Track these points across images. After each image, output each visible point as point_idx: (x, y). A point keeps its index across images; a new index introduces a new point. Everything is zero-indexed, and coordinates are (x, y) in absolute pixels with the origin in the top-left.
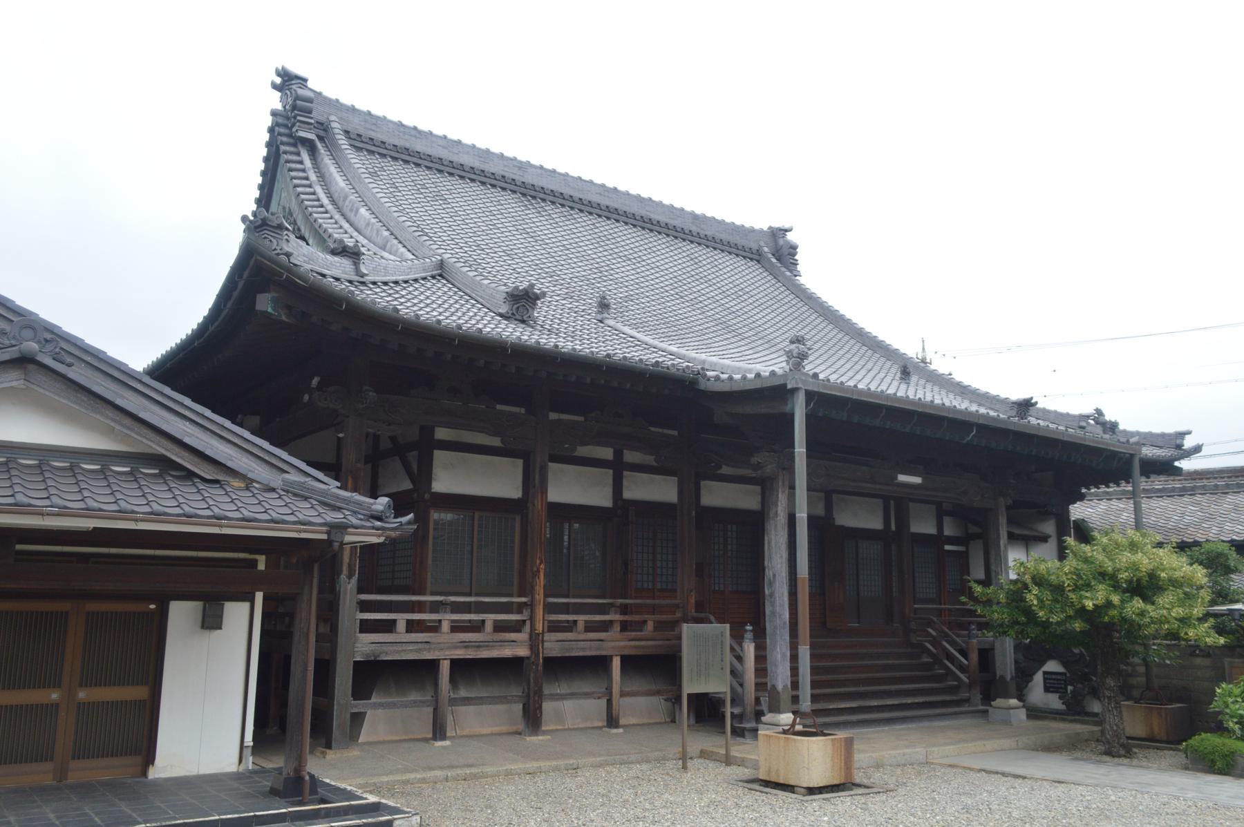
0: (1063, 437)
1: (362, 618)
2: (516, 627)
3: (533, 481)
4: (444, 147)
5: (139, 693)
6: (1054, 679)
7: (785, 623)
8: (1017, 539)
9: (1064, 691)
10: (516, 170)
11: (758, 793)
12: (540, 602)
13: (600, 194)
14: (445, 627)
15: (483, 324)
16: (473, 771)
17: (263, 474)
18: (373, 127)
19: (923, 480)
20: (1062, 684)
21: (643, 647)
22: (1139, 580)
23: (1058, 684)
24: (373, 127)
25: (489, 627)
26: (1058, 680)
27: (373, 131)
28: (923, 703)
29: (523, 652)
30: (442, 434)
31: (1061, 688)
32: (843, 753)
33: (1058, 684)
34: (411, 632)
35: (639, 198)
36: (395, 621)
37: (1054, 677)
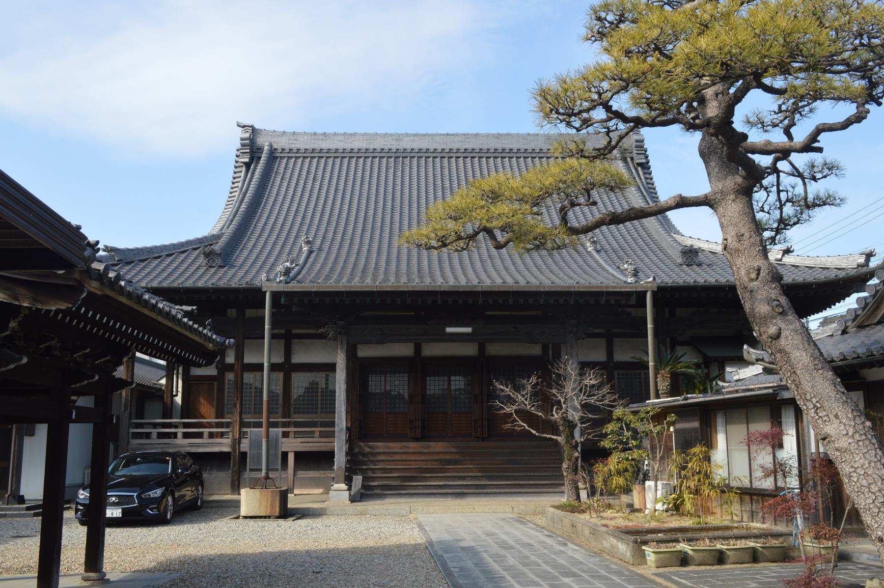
2: (222, 435)
3: (418, 348)
4: (342, 141)
7: (342, 429)
8: (734, 360)
10: (394, 142)
12: (236, 420)
13: (462, 142)
14: (180, 435)
16: (615, 541)
18: (295, 142)
19: (444, 330)
21: (316, 447)
24: (295, 142)
25: (206, 435)
27: (294, 144)
28: (170, 428)
29: (226, 449)
30: (295, 331)
32: (269, 499)
35: (498, 136)
36: (151, 433)
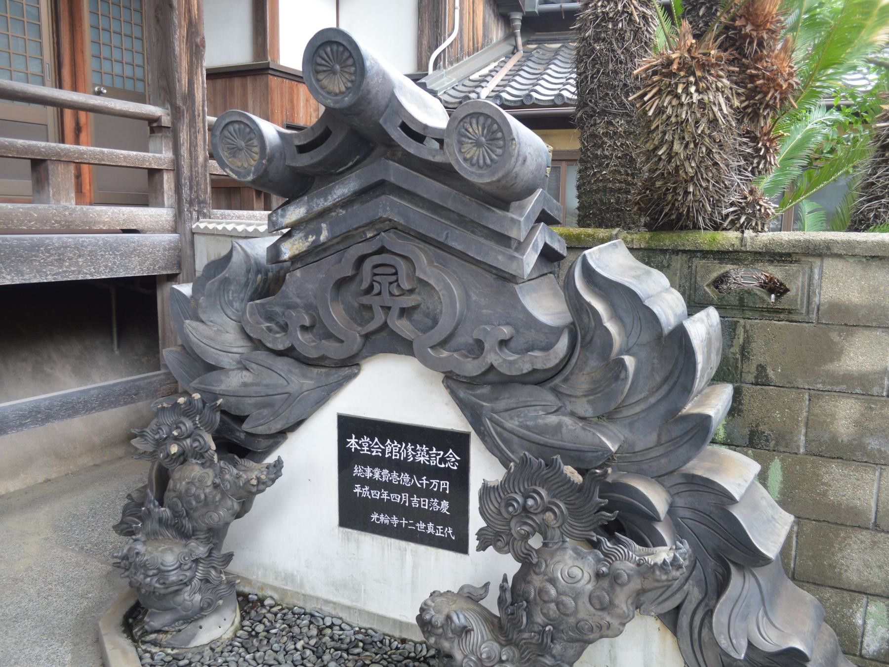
0: (150, 164)
1: (161, 209)
5: (88, 200)
6: (399, 466)
9: (357, 471)
11: (92, 162)
15: (233, 505)
17: (746, 285)
20: (441, 496)
22: (579, 216)
23: (413, 491)
26: (416, 469)
31: (437, 518)
33: (413, 491)
34: (541, 213)
37: (393, 449)
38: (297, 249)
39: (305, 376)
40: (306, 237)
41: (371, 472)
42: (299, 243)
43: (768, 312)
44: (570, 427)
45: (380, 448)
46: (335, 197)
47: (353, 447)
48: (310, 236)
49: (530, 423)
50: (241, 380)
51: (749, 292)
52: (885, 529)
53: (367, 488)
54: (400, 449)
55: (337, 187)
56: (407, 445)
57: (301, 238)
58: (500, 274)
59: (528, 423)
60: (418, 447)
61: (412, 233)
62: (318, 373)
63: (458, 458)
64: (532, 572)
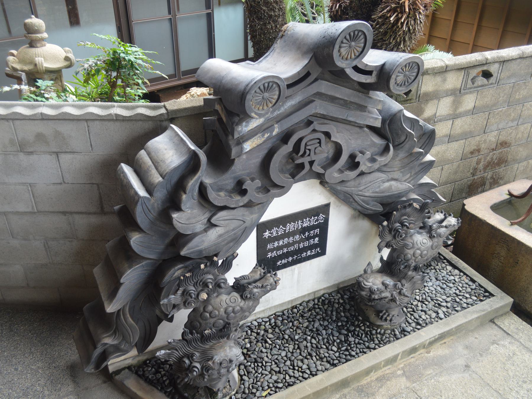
38: (256, 144)
39: (252, 213)
40: (263, 135)
41: (278, 243)
42: (257, 140)
43: (404, 101)
44: (395, 185)
45: (283, 229)
46: (286, 107)
47: (267, 236)
48: (266, 134)
49: (377, 190)
50: (217, 234)
51: (399, 95)
52: (391, 162)
53: (275, 252)
54: (294, 225)
55: (288, 101)
56: (298, 222)
57: (259, 137)
58: (359, 125)
59: (376, 190)
60: (304, 220)
61: (318, 116)
62: (258, 209)
63: (324, 216)
64: (405, 248)
